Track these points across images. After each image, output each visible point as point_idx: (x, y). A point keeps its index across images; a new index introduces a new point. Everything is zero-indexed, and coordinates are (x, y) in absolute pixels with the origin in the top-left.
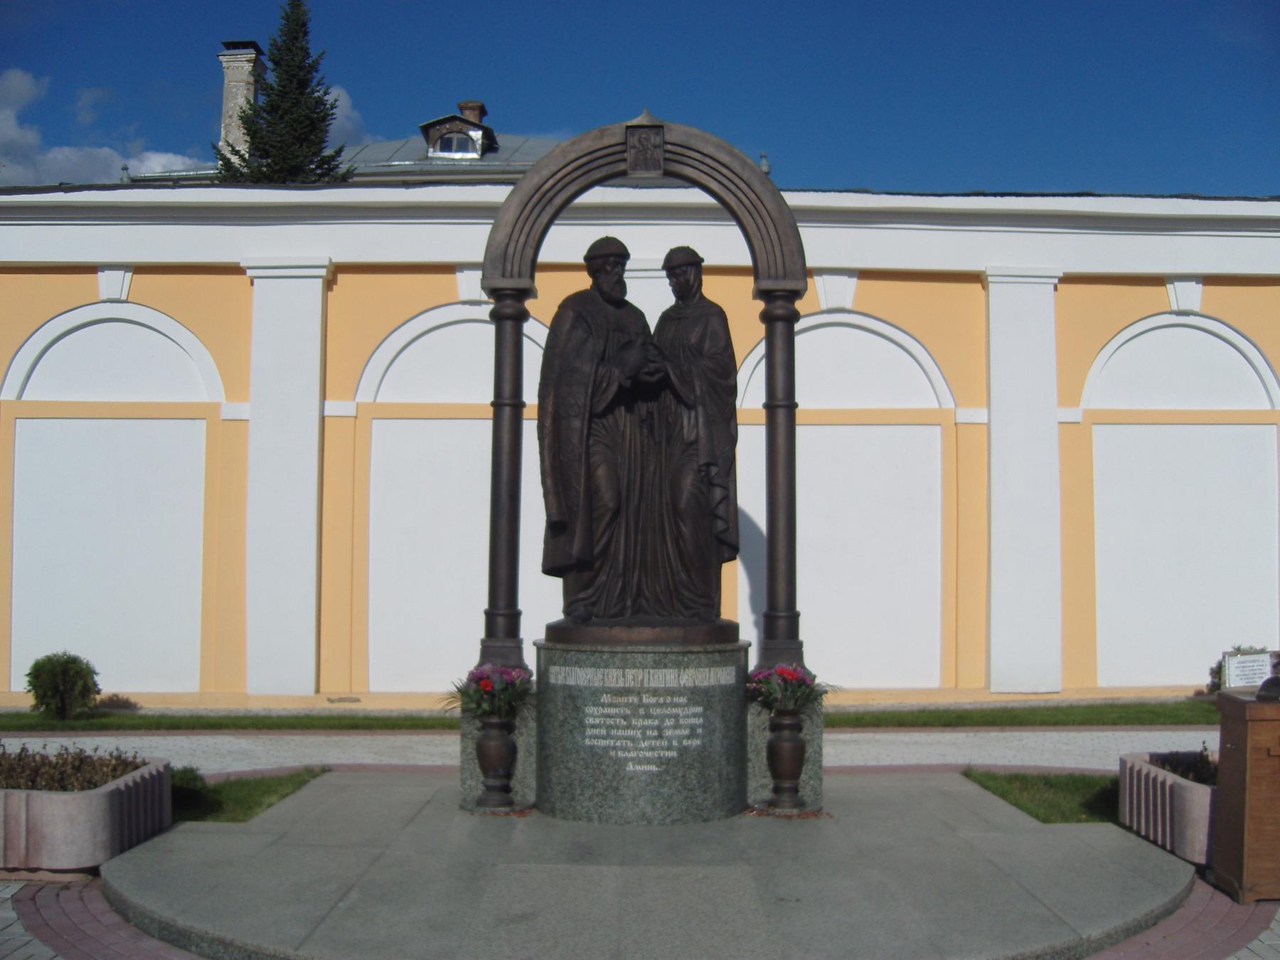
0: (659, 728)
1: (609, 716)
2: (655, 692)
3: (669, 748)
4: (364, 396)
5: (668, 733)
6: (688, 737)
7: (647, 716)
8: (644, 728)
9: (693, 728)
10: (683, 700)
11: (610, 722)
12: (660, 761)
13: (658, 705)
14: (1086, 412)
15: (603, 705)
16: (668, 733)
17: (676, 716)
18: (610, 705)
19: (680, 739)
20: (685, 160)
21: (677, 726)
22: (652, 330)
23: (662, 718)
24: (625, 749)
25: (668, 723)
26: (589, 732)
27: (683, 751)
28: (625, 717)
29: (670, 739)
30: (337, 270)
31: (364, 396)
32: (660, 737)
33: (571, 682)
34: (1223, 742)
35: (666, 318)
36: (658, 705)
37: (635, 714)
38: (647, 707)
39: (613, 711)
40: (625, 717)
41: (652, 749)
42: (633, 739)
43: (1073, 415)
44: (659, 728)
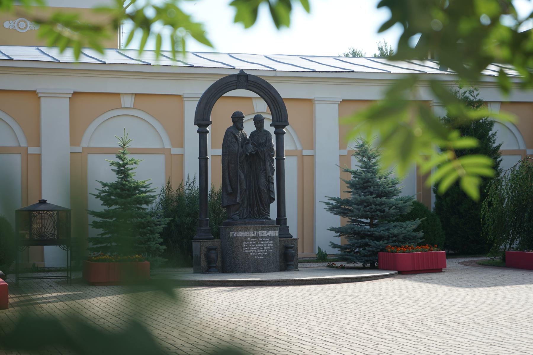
0: (263, 247)
1: (250, 244)
2: (262, 237)
3: (265, 252)
4: (84, 144)
5: (265, 248)
6: (270, 249)
7: (260, 244)
8: (259, 247)
9: (271, 247)
10: (268, 239)
11: (250, 245)
12: (264, 255)
13: (262, 241)
14: (349, 151)
15: (248, 241)
16: (265, 248)
17: (267, 244)
18: (250, 241)
19: (268, 249)
20: (273, 98)
21: (267, 246)
22: (248, 138)
23: (263, 244)
24: (255, 252)
25: (265, 245)
26: (244, 249)
27: (269, 252)
28: (254, 244)
29: (265, 250)
30: (75, 93)
31: (84, 144)
32: (263, 249)
33: (238, 236)
34: (451, 68)
35: (252, 134)
36: (262, 241)
37: (257, 243)
38: (260, 241)
39: (251, 243)
40: (254, 244)
41: (261, 252)
42: (256, 250)
43: (345, 152)
44: (263, 247)
